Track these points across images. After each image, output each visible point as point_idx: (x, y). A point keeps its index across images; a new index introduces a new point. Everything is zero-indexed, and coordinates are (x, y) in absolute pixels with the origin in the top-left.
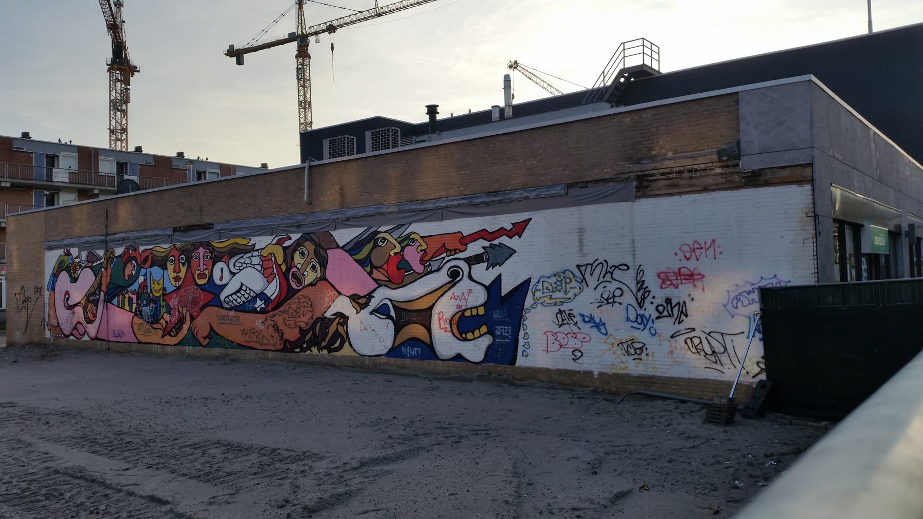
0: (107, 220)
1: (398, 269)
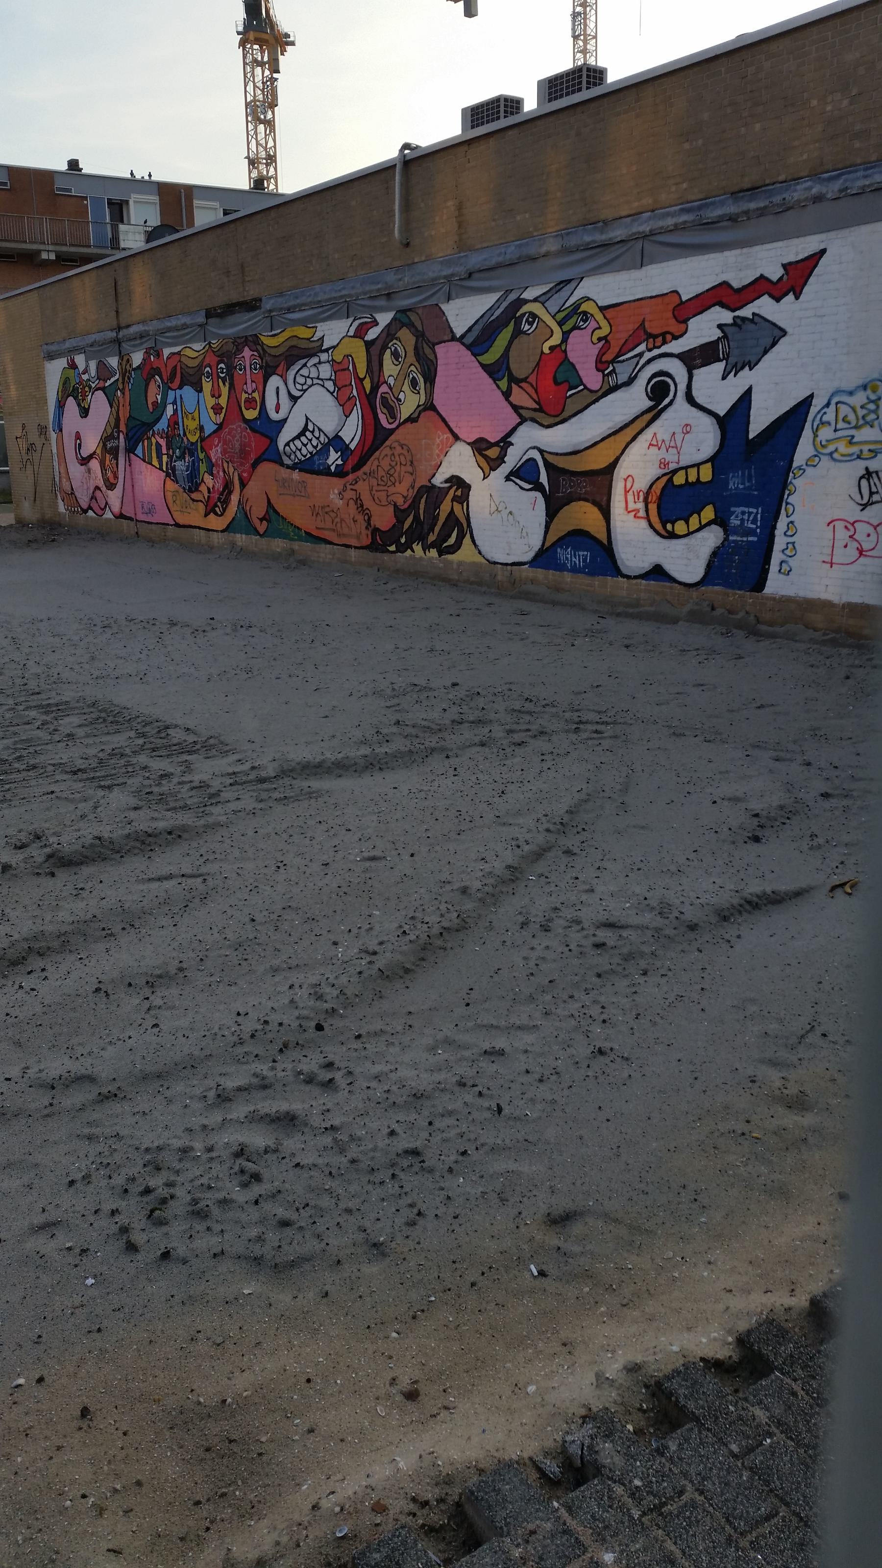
0: (116, 301)
1: (556, 382)
